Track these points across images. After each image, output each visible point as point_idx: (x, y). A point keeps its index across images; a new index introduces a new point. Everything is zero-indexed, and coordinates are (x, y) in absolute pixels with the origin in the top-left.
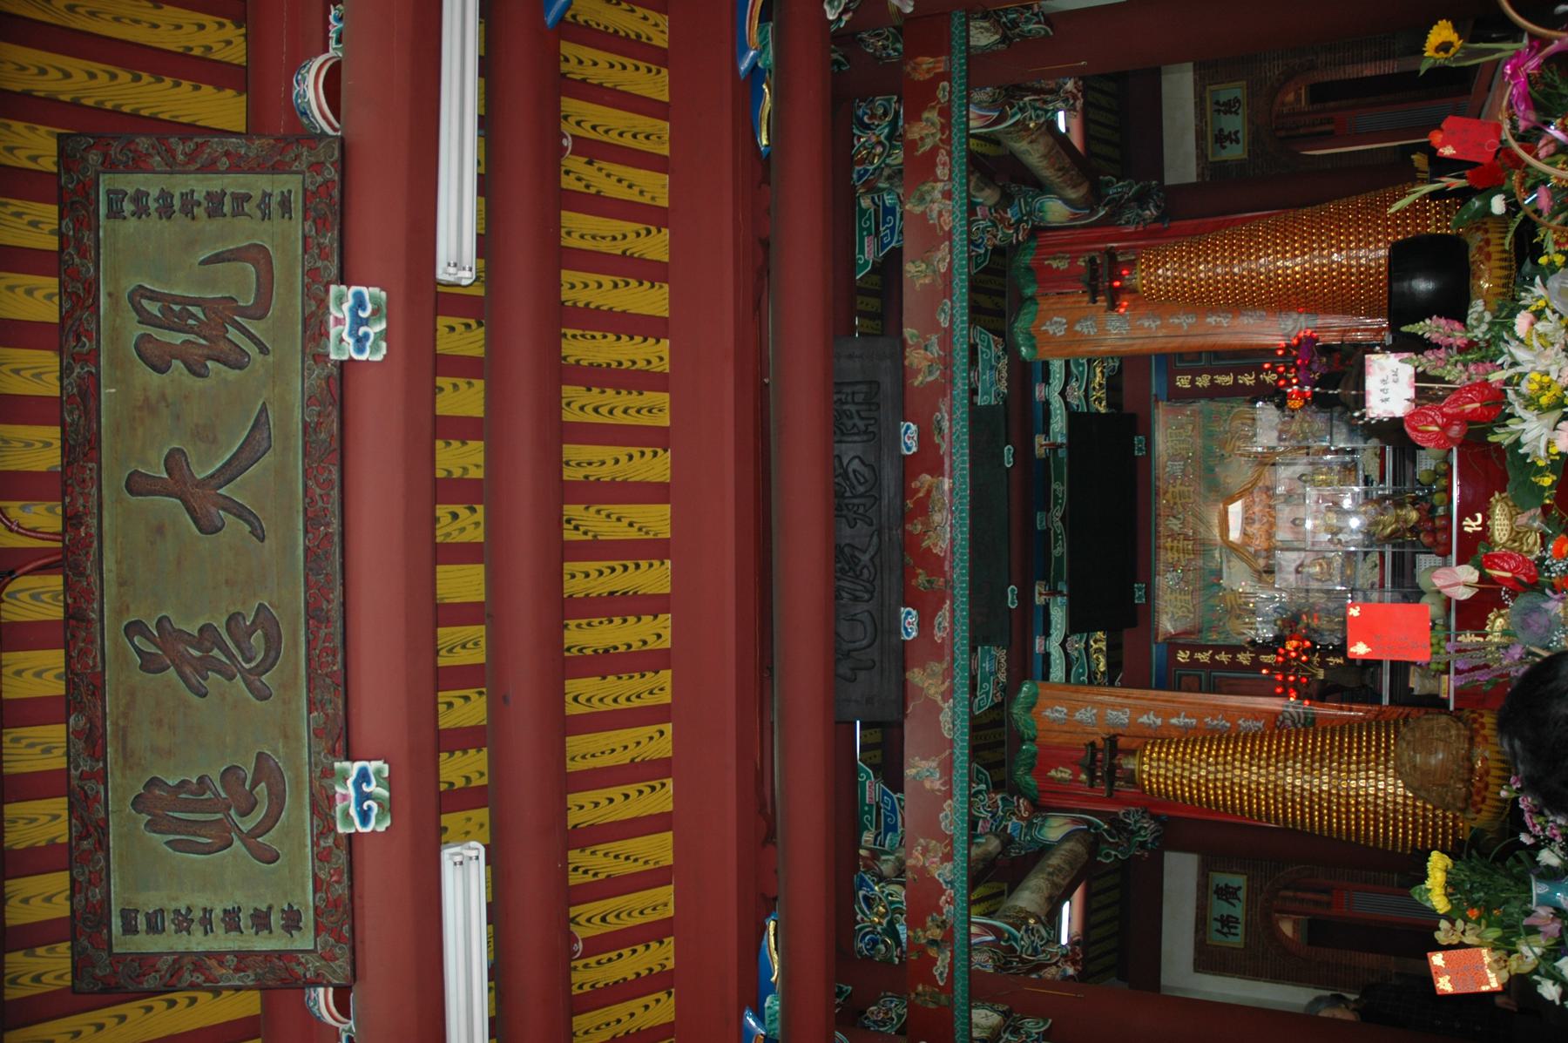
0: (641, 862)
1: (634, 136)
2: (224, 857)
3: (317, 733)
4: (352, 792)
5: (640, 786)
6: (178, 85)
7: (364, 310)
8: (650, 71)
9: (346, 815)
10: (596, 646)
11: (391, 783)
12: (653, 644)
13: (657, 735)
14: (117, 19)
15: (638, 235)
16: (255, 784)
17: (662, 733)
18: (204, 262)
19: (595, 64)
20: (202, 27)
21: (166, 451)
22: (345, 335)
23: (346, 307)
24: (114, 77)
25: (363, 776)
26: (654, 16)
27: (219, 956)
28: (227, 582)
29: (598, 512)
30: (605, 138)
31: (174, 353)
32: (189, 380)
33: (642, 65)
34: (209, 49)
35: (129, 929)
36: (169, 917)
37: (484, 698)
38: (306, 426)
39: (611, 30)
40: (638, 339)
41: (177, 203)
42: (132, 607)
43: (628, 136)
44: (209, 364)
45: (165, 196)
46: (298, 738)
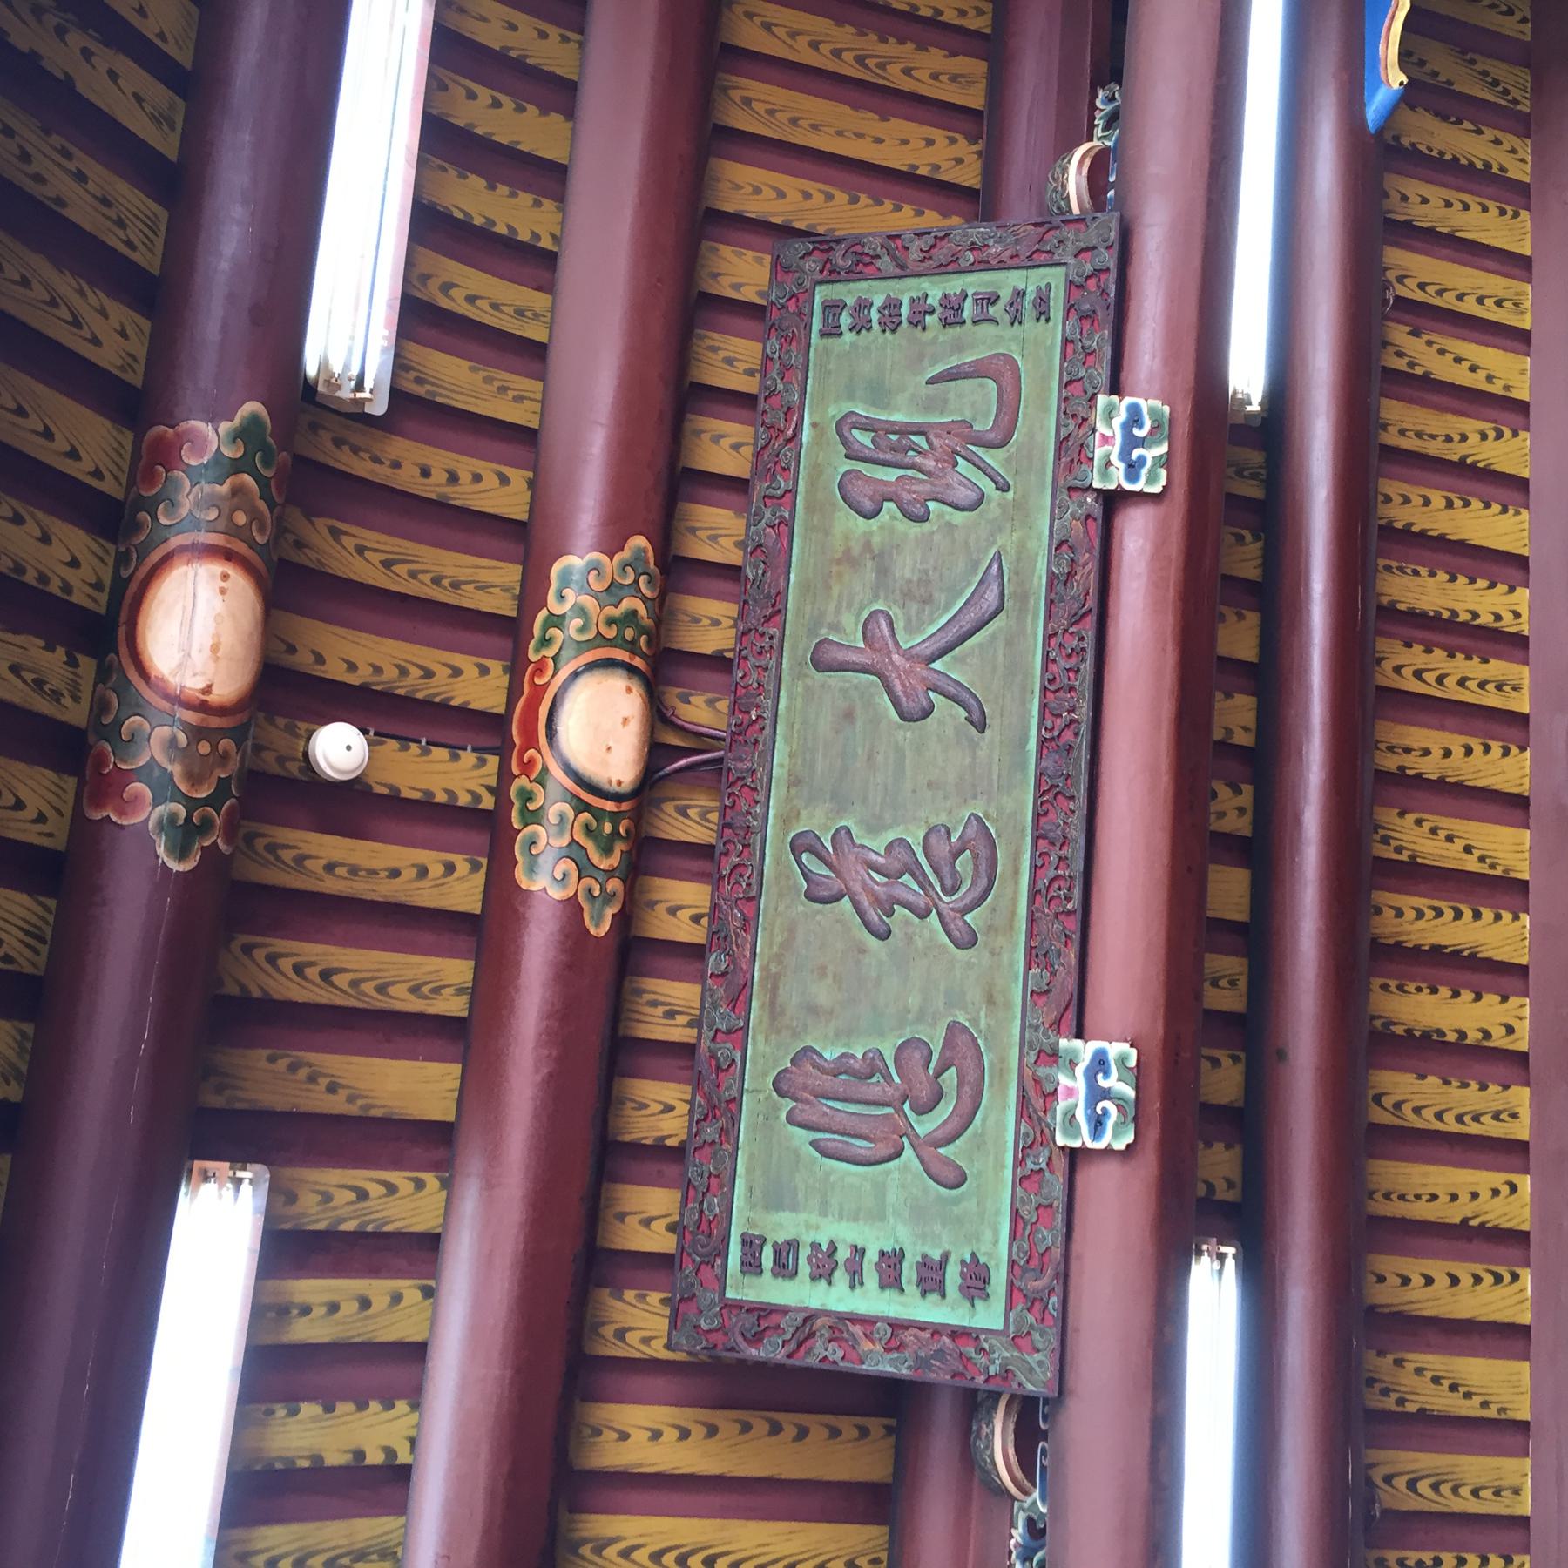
0: (1477, 1400)
1: (1480, 300)
2: (888, 1173)
3: (1035, 995)
4: (1080, 1085)
5: (1479, 1269)
6: (898, 208)
7: (1141, 427)
8: (1503, 212)
9: (1070, 1118)
10: (1412, 1024)
11: (1139, 1076)
12: (1499, 1040)
13: (1505, 1190)
14: (840, 133)
15: (1484, 437)
16: (940, 1072)
17: (1513, 1188)
18: (929, 382)
19: (1425, 201)
20: (930, 143)
21: (865, 614)
22: (1114, 458)
23: (1117, 422)
24: (829, 197)
25: (1100, 1063)
26: (1509, 140)
27: (867, 1321)
28: (930, 784)
29: (1419, 822)
30: (1437, 302)
31: (886, 495)
32: (903, 525)
33: (1492, 205)
34: (937, 167)
35: (751, 1265)
36: (804, 1252)
37: (1241, 1067)
38: (1052, 578)
39: (1448, 157)
40: (1482, 583)
41: (905, 311)
42: (804, 813)
43: (1470, 300)
44: (931, 505)
45: (892, 306)
46: (1008, 1005)
